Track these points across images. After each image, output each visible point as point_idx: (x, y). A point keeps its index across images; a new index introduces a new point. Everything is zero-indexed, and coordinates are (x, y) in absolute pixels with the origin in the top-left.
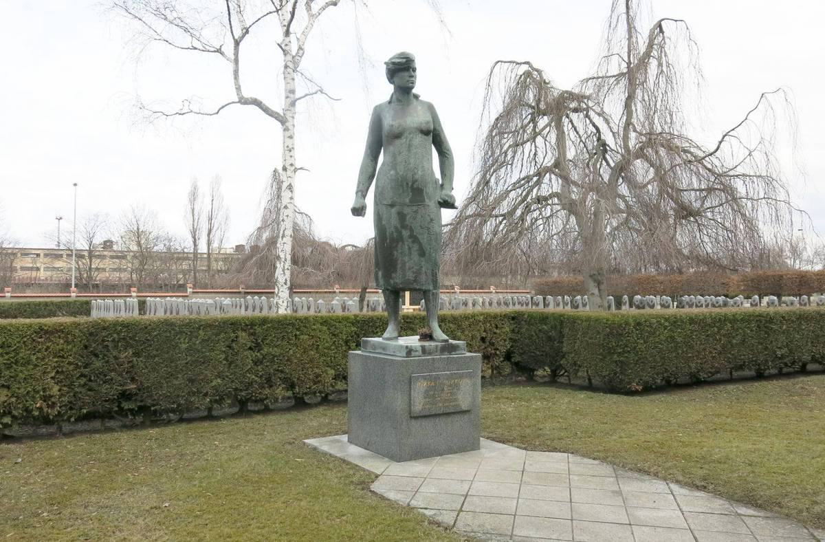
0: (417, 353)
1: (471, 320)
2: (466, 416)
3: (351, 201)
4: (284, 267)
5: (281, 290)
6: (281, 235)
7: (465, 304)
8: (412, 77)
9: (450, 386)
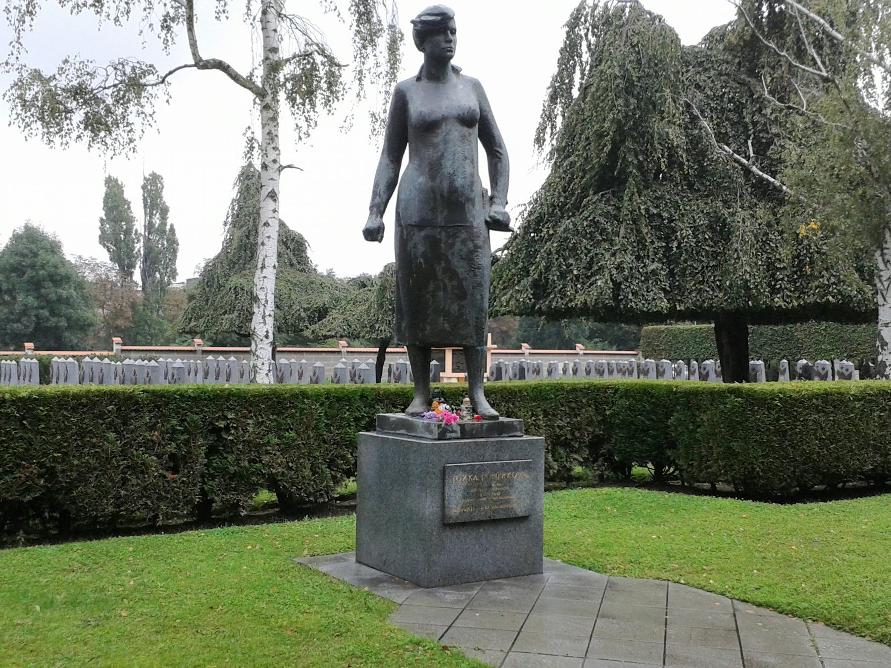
0: (454, 435)
1: (539, 394)
2: (523, 526)
3: (362, 218)
4: (264, 313)
5: (260, 346)
6: (260, 265)
7: (537, 371)
8: (451, 41)
9: (501, 481)
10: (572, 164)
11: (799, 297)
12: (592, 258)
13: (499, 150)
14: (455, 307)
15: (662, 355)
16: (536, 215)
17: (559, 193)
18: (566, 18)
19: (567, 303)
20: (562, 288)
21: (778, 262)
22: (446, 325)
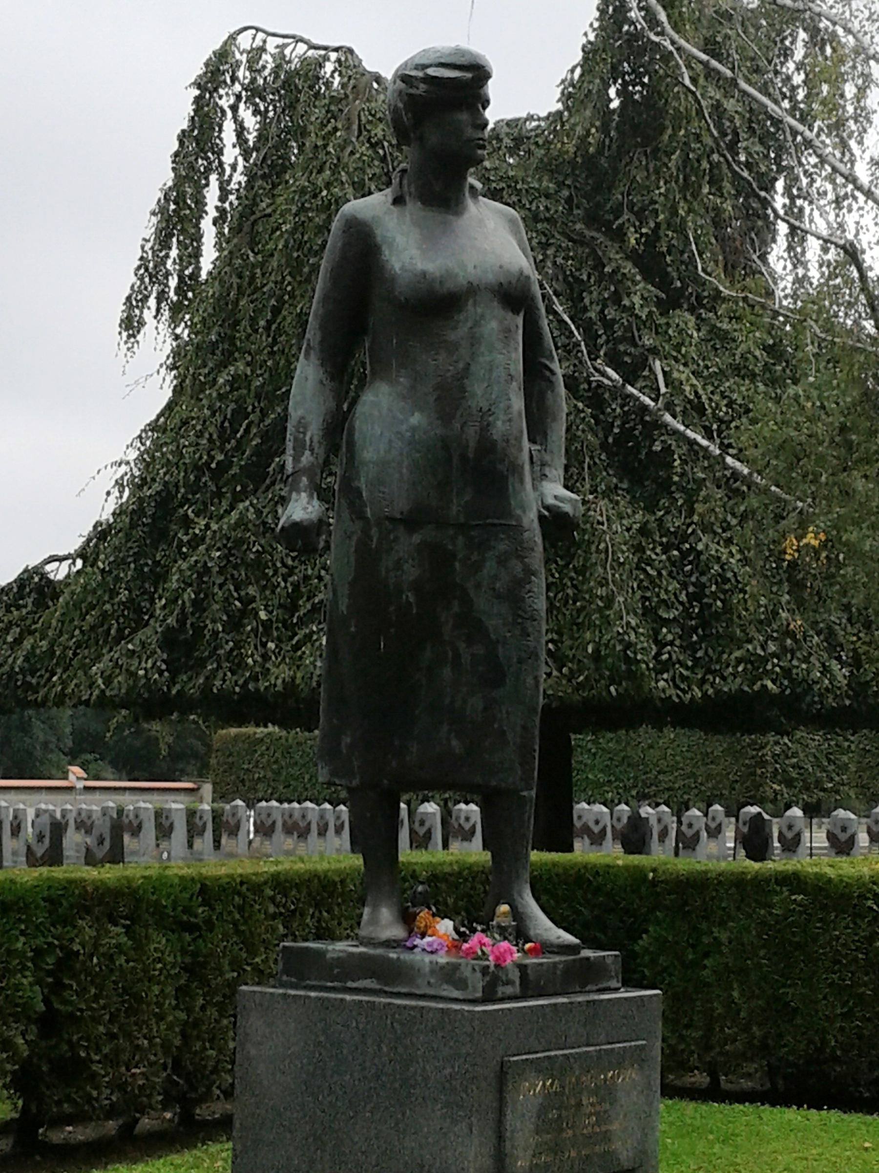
10: (235, 382)
11: (703, 681)
12: (296, 586)
13: (548, 363)
14: (476, 702)
15: (256, 790)
16: (157, 487)
17: (210, 440)
18: (198, 69)
19: (246, 683)
20: (232, 650)
21: (663, 607)
22: (454, 743)
